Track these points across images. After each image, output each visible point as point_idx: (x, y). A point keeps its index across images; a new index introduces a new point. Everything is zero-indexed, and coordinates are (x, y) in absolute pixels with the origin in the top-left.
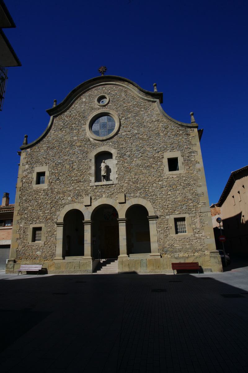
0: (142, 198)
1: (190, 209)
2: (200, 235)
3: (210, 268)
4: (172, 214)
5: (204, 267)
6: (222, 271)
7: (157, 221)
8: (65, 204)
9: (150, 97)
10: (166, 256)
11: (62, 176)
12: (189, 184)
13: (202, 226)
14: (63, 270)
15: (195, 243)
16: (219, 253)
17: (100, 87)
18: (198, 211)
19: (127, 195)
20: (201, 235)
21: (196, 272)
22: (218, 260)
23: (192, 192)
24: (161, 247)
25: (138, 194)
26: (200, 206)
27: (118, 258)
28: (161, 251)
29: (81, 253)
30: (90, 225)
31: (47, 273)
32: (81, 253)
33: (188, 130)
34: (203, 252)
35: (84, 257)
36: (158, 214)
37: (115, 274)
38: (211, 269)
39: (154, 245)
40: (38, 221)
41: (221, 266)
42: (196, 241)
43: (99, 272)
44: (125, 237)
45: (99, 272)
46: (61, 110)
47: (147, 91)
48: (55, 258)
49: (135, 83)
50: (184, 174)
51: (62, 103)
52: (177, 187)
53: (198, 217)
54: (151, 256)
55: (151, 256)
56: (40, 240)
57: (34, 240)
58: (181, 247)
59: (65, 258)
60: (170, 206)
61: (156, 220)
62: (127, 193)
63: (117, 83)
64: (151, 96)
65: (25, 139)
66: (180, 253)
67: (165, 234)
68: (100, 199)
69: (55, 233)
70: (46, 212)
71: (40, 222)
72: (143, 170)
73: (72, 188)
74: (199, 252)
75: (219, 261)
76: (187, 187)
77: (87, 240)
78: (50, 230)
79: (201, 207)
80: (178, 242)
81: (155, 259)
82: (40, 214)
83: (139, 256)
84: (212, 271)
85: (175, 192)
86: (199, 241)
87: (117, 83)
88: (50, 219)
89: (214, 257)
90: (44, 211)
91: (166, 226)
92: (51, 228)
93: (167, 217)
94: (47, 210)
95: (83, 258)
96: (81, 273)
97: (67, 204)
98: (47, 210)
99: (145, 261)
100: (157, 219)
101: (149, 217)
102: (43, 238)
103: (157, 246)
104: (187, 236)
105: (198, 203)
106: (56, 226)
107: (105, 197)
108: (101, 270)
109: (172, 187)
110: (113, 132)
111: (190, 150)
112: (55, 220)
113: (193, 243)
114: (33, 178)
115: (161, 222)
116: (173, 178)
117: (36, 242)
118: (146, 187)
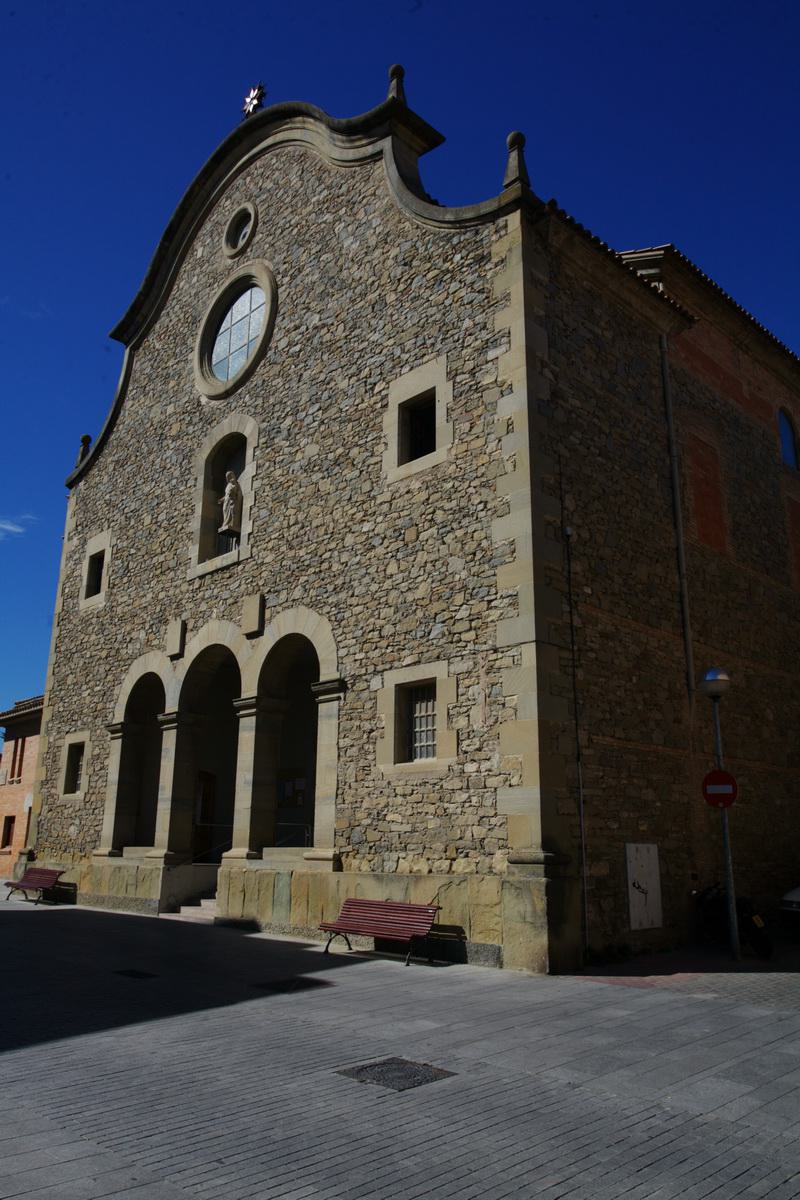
0: (307, 605)
1: (456, 638)
2: (485, 766)
3: (496, 943)
4: (391, 668)
5: (474, 938)
6: (541, 970)
7: (342, 702)
8: (133, 658)
9: (364, 142)
10: (355, 863)
12: (463, 512)
13: (492, 720)
14: (101, 894)
15: (459, 810)
16: (541, 868)
17: (239, 181)
18: (485, 643)
19: (271, 600)
20: (487, 765)
22: (534, 906)
23: (472, 550)
24: (344, 824)
25: (297, 593)
26: (494, 614)
27: (223, 860)
28: (342, 841)
29: (148, 840)
30: (120, 740)
31: (74, 903)
32: (148, 840)
33: (486, 233)
34: (487, 860)
35: (308, 852)
37: (203, 922)
38: (499, 948)
39: (325, 815)
41: (544, 939)
42: (465, 796)
43: (188, 914)
45: (188, 914)
46: (146, 318)
47: (344, 121)
48: (95, 852)
49: (315, 107)
50: (451, 463)
51: (141, 293)
52: (418, 534)
53: (482, 672)
54: (307, 859)
55: (307, 859)
56: (431, 751)
57: (406, 750)
58: (408, 828)
59: (261, 852)
60: (388, 630)
61: (339, 698)
62: (269, 591)
63: (280, 137)
66: (403, 855)
67: (362, 763)
72: (321, 482)
74: (472, 853)
75: (534, 911)
76: (455, 525)
79: (501, 617)
80: (400, 799)
81: (314, 876)
83: (287, 858)
84: (499, 962)
85: (412, 558)
86: (474, 800)
87: (280, 137)
89: (520, 889)
90: (92, 688)
91: (367, 726)
93: (375, 683)
95: (149, 854)
99: (284, 881)
100: (342, 695)
101: (321, 688)
102: (445, 739)
103: (333, 819)
104: (432, 772)
105: (490, 602)
107: (217, 617)
108: (199, 905)
109: (403, 540)
111: (484, 335)
113: (451, 808)
115: (355, 706)
116: (410, 495)
117: (417, 761)
118: (323, 557)
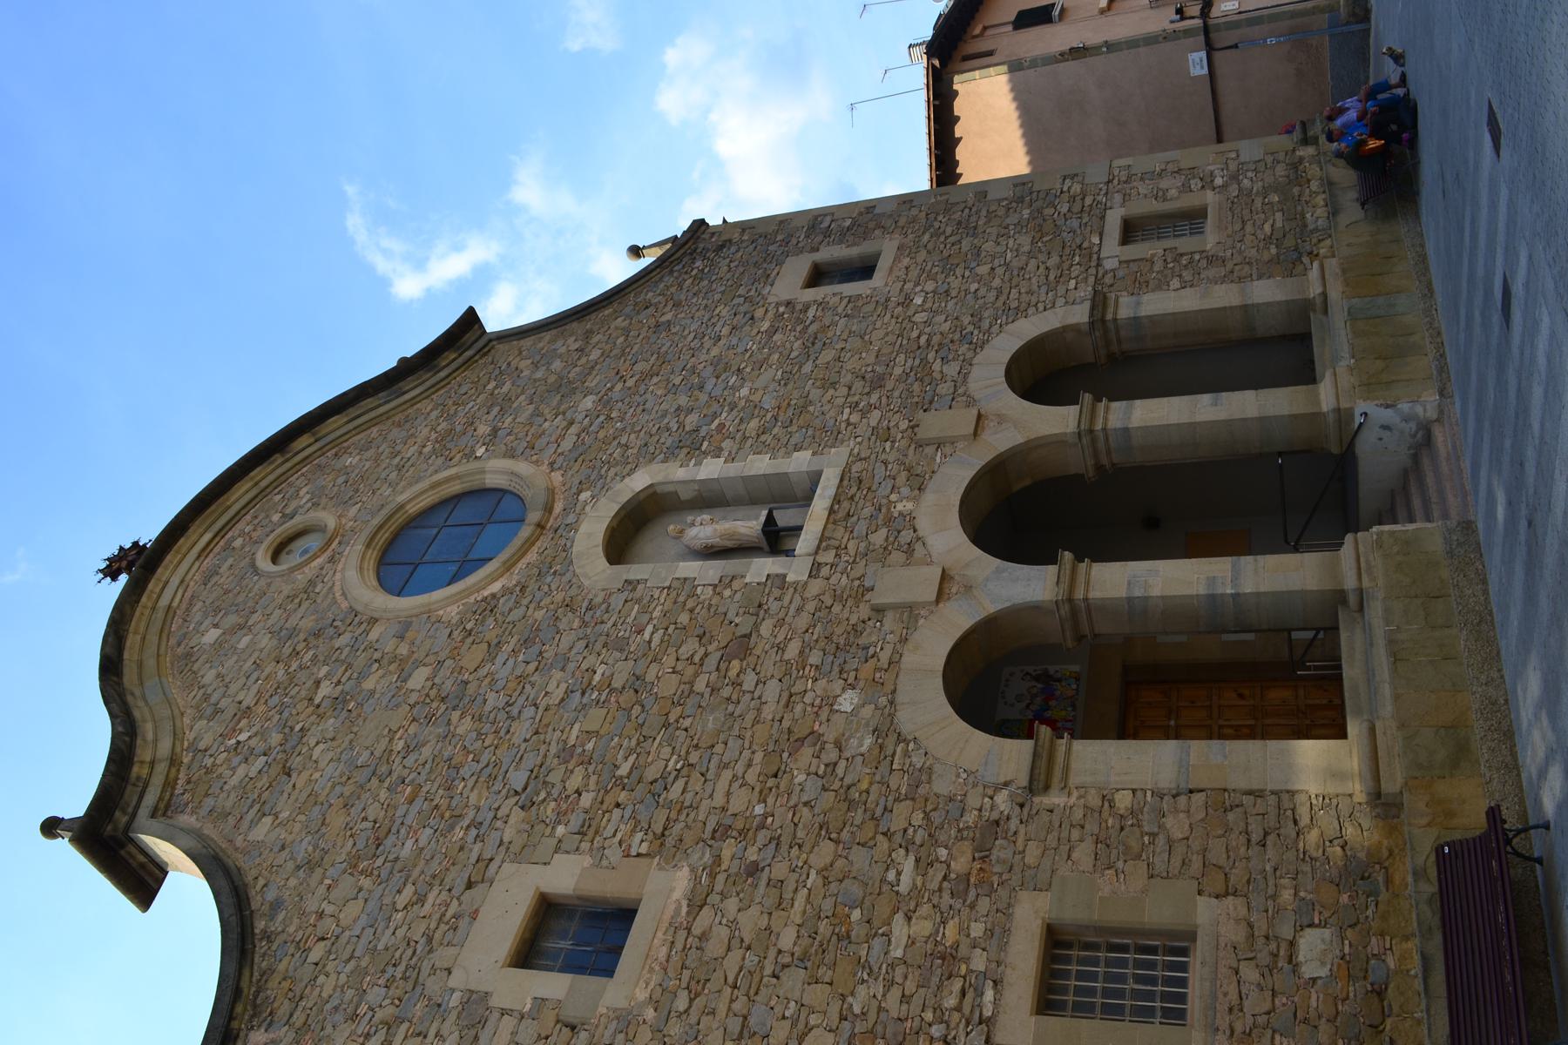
8: (886, 730)
11: (642, 760)
21: (1384, 91)
36: (1086, 291)
40: (979, 962)
44: (1206, 398)
64: (429, 371)
65: (1325, 702)
68: (920, 524)
69: (1123, 801)
70: (903, 888)
71: (999, 933)
73: (772, 690)
77: (1212, 581)
78: (1089, 841)
82: (911, 942)
88: (982, 853)
92: (1076, 834)
94: (891, 876)
96: (805, 540)
97: (892, 716)
98: (891, 876)
106: (1055, 799)
110: (464, 485)
112: (1002, 799)
114: (540, 1002)
